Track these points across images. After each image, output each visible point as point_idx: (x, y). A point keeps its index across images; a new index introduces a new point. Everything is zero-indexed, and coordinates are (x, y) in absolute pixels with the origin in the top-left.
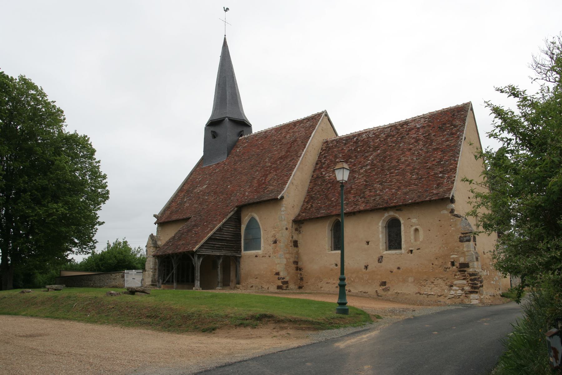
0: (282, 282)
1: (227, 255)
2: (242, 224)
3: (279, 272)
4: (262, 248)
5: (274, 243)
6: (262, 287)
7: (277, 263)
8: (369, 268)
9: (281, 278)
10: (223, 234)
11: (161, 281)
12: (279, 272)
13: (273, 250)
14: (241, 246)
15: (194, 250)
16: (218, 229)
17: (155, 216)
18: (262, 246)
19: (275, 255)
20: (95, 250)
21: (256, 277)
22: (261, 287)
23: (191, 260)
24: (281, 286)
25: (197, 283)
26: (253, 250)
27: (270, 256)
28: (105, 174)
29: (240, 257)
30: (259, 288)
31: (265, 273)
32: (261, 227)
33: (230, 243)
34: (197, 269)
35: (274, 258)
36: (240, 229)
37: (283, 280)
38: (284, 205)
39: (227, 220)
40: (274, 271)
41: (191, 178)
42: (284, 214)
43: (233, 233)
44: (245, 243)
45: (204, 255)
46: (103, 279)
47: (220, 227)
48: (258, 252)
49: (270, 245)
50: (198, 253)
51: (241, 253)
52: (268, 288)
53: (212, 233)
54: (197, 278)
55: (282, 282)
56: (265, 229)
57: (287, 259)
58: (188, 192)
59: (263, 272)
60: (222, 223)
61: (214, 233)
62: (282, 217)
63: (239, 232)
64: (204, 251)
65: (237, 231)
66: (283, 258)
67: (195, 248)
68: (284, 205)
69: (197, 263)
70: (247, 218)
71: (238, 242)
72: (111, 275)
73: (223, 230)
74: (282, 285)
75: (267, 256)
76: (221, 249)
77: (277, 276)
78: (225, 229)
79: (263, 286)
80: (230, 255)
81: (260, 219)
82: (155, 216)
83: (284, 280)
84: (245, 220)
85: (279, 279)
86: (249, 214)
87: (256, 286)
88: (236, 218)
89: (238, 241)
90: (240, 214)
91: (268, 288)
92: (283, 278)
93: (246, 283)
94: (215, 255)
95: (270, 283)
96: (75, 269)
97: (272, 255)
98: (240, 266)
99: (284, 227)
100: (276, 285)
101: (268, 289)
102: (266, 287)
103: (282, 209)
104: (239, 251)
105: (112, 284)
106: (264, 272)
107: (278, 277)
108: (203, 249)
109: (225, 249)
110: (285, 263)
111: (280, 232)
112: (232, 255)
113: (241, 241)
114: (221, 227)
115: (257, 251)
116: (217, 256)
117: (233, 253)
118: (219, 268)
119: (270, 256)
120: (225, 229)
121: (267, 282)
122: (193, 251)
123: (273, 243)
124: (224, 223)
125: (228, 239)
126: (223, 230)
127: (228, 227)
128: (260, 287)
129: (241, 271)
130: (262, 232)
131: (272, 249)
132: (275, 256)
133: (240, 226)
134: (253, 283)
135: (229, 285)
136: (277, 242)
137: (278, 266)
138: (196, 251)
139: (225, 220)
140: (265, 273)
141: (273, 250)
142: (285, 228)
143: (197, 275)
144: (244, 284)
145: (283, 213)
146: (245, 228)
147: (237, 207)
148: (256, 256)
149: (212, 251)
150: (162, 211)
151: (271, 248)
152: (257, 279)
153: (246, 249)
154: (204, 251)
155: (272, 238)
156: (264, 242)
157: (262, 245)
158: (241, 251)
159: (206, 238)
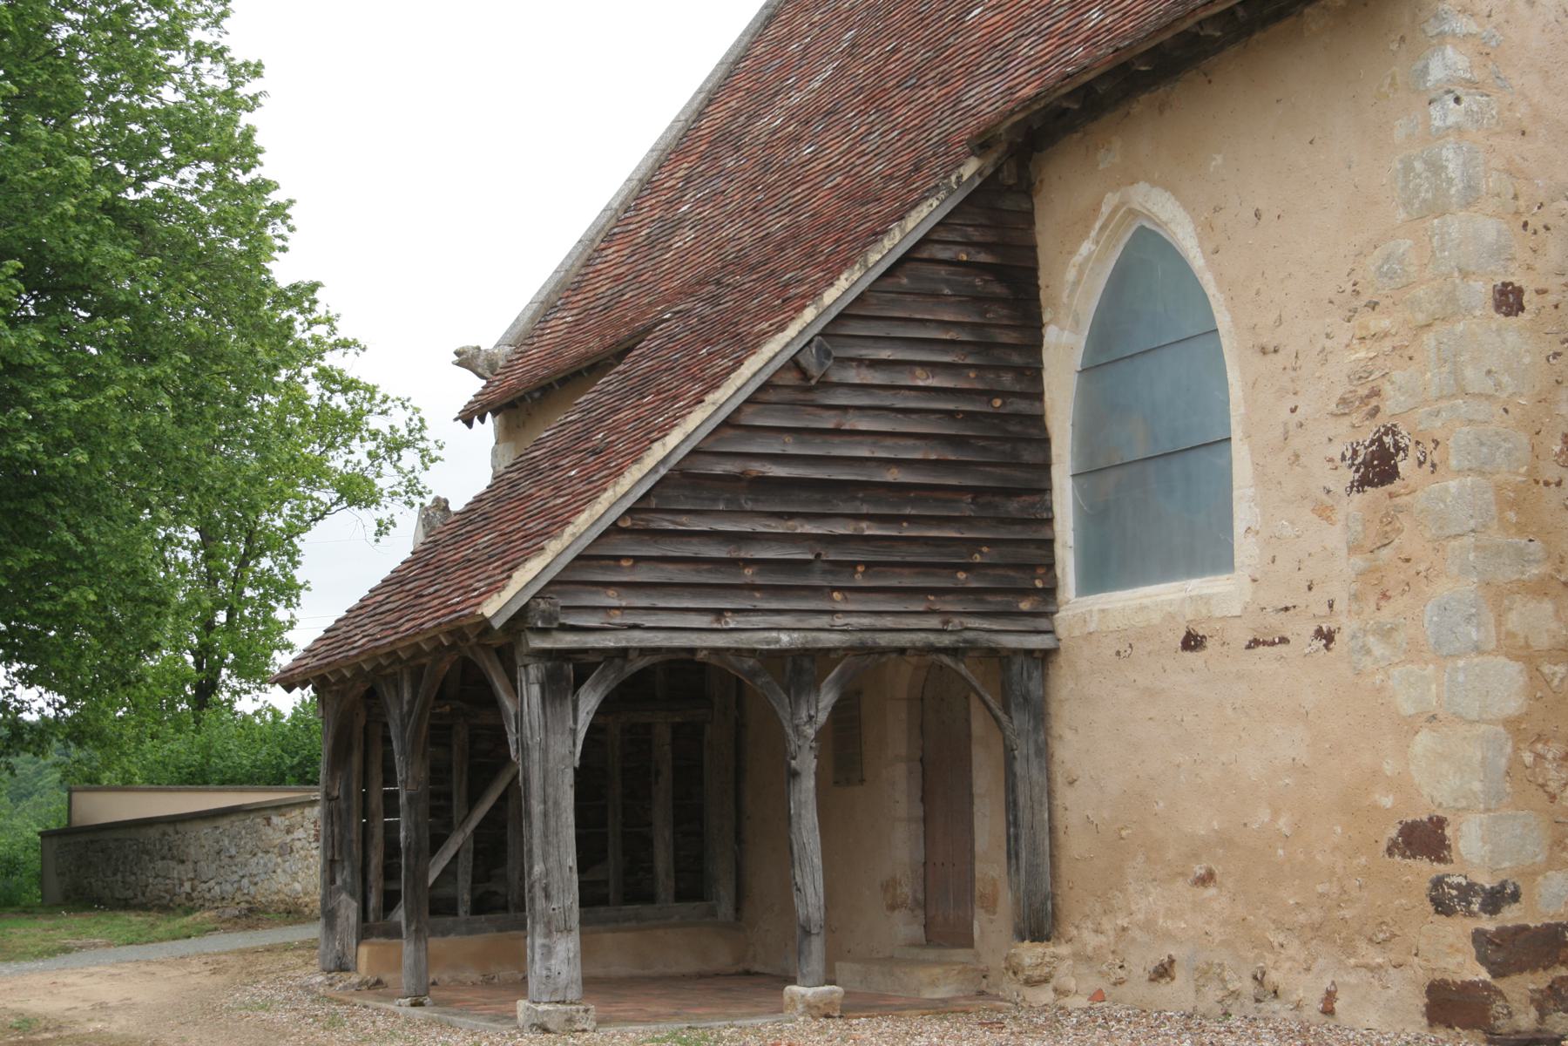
0: (1479, 937)
1: (884, 640)
2: (1046, 317)
3: (1439, 823)
4: (1245, 549)
5: (1363, 483)
6: (1266, 990)
7: (1408, 708)
8: (1257, 576)
9: (1467, 891)
10: (837, 432)
11: (349, 909)
12: (1439, 823)
13: (1359, 561)
14: (1049, 543)
15: (489, 608)
16: (766, 386)
17: (466, 359)
18: (1239, 528)
19: (1387, 615)
20: (1542, 642)
21: (1199, 870)
22: (1258, 979)
23: (494, 703)
24: (1468, 987)
25: (548, 952)
26: (1168, 572)
27: (1327, 637)
28: (247, 125)
29: (1044, 658)
30: (1235, 994)
31: (1283, 824)
32: (1223, 321)
33: (912, 520)
34: (537, 808)
35: (1379, 649)
36: (1034, 373)
37: (1489, 924)
38: (1462, 25)
39: (872, 288)
40: (1387, 801)
41: (759, 50)
42: (1459, 129)
43: (950, 414)
44: (1093, 516)
45: (623, 653)
46: (233, 851)
47: (794, 363)
48: (1206, 599)
49: (1324, 512)
50: (537, 643)
51: (1048, 615)
52: (1330, 997)
53: (696, 421)
54: (540, 903)
55: (1479, 937)
56: (1268, 340)
57: (1528, 657)
58: (727, 139)
59: (1264, 815)
60: (809, 314)
61: (727, 423)
62: (1436, 167)
63: (1022, 406)
64: (618, 619)
65: (990, 394)
66: (1478, 649)
67: (495, 588)
68: (1462, 25)
69: (545, 751)
70: (1086, 248)
71: (1013, 506)
72: (268, 821)
73: (825, 385)
74: (1483, 975)
75: (1301, 630)
76: (816, 581)
77: (1425, 869)
78: (853, 376)
79: (1274, 977)
80: (919, 639)
81: (1206, 230)
82: (466, 359)
83: (1511, 916)
84: (1071, 275)
85: (1442, 906)
86: (1105, 210)
87: (1205, 974)
88: (983, 257)
89: (1010, 493)
90: (1028, 217)
91: (1330, 997)
92: (1496, 899)
93: (1107, 925)
94: (753, 652)
95: (1348, 948)
96: (258, 779)
97: (1346, 625)
98: (1044, 753)
99: (1465, 274)
100: (1419, 973)
101: (1328, 1011)
102: (1309, 991)
103: (1437, 72)
104: (1025, 592)
105: (275, 887)
106: (1276, 813)
107: (1438, 882)
108: (611, 599)
109: (859, 580)
110: (1513, 705)
111: (1429, 339)
112: (946, 640)
113: (1042, 489)
114: (810, 361)
115: (1197, 586)
116: (773, 659)
117: (956, 623)
118: (808, 784)
119: (1327, 637)
120: (853, 376)
121: (1316, 928)
122: (485, 624)
123: (1351, 475)
124: (842, 317)
125: (894, 475)
126: (825, 385)
127: (885, 354)
128: (1248, 986)
129: (1066, 797)
130: (1233, 376)
131: (1353, 549)
132: (1386, 633)
133: (1034, 346)
134: (1169, 936)
135: (967, 941)
136: (1404, 466)
137: (1424, 740)
138: (519, 621)
139: (842, 283)
140: (1283, 824)
141: (1359, 561)
142: (1481, 290)
143: (538, 869)
144: (1091, 940)
145: (1446, 114)
146: (1077, 361)
147: (981, 144)
148: (1192, 642)
149: (719, 613)
150: (526, 318)
151: (1335, 537)
152: (1211, 891)
153: (1096, 578)
154: (618, 619)
155: (1342, 428)
156: (1261, 474)
157: (1244, 513)
158: (1050, 592)
159: (632, 481)
